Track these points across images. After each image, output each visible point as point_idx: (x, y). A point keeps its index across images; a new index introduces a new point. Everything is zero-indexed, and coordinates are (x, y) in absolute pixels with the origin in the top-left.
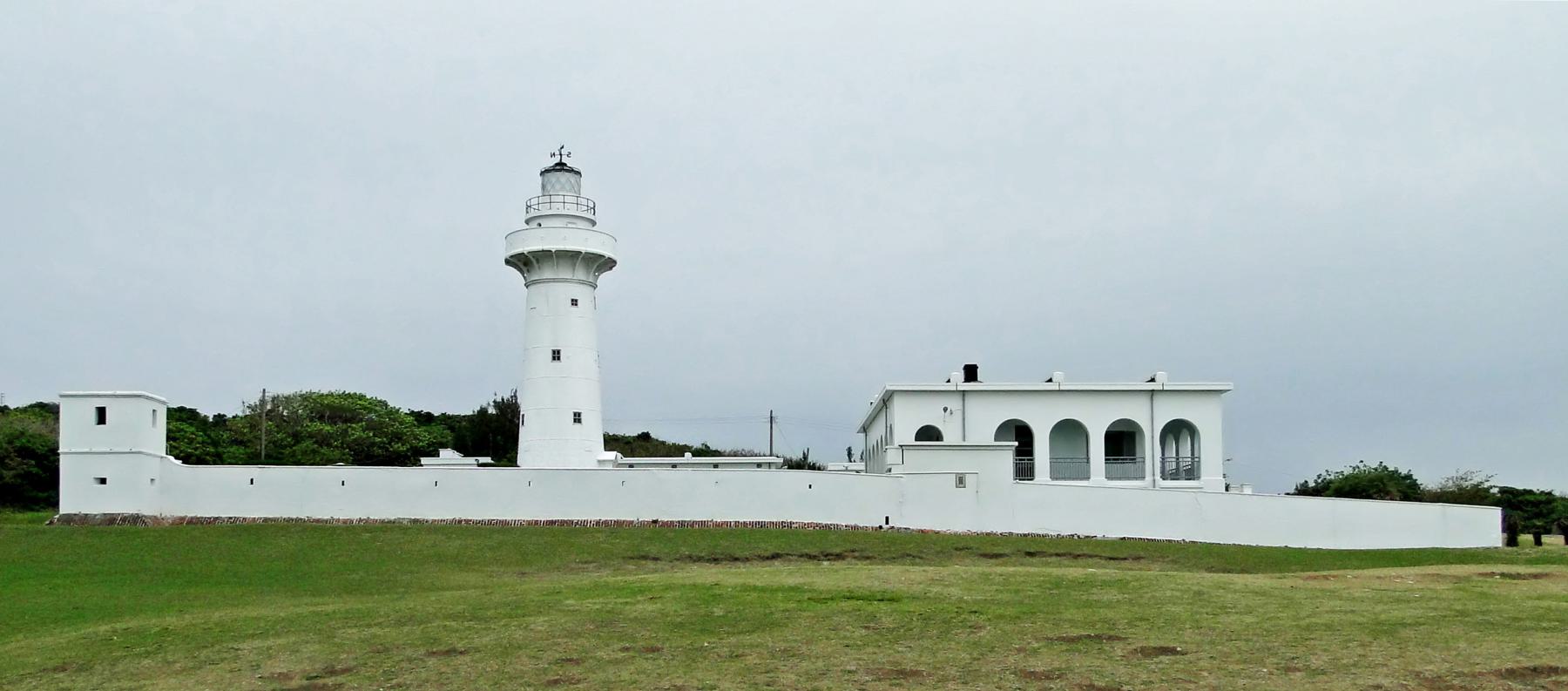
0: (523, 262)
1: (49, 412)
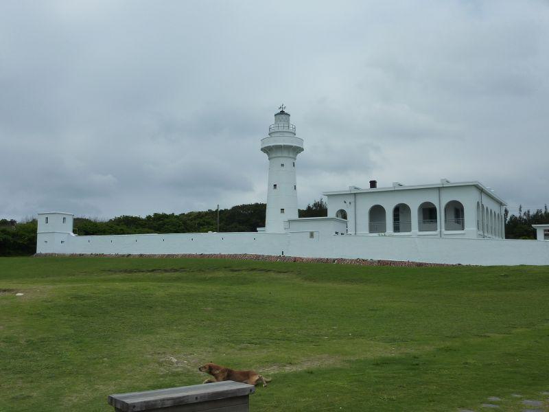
0: (267, 150)
1: (34, 222)
